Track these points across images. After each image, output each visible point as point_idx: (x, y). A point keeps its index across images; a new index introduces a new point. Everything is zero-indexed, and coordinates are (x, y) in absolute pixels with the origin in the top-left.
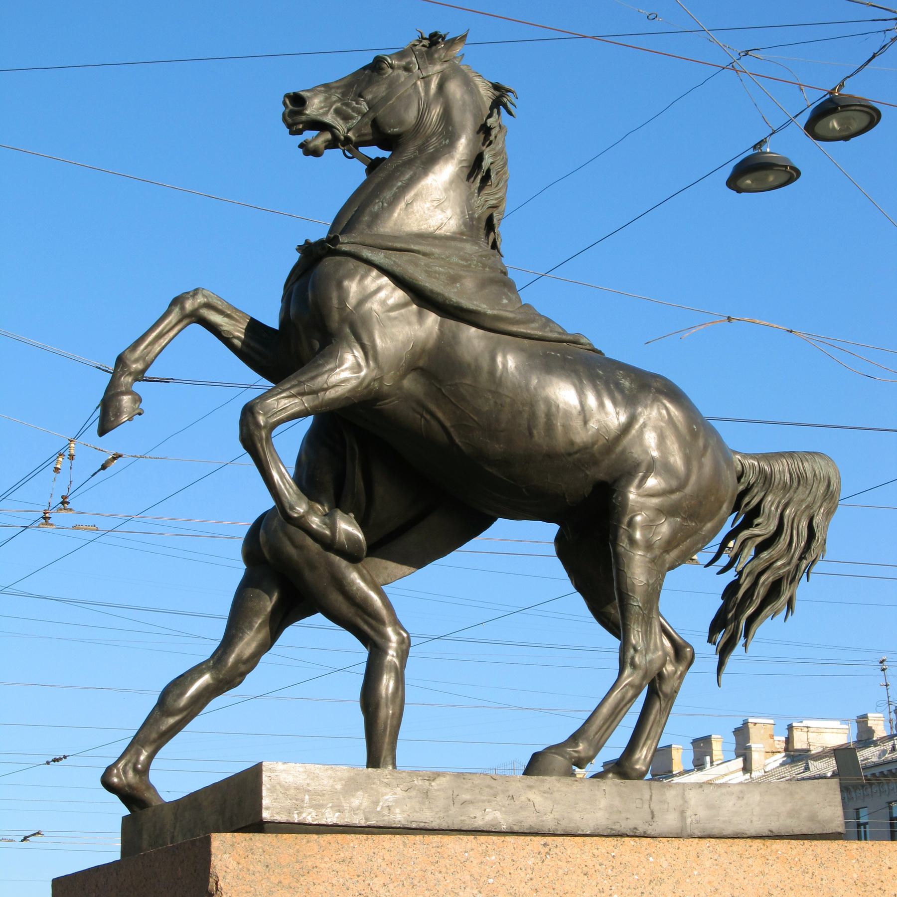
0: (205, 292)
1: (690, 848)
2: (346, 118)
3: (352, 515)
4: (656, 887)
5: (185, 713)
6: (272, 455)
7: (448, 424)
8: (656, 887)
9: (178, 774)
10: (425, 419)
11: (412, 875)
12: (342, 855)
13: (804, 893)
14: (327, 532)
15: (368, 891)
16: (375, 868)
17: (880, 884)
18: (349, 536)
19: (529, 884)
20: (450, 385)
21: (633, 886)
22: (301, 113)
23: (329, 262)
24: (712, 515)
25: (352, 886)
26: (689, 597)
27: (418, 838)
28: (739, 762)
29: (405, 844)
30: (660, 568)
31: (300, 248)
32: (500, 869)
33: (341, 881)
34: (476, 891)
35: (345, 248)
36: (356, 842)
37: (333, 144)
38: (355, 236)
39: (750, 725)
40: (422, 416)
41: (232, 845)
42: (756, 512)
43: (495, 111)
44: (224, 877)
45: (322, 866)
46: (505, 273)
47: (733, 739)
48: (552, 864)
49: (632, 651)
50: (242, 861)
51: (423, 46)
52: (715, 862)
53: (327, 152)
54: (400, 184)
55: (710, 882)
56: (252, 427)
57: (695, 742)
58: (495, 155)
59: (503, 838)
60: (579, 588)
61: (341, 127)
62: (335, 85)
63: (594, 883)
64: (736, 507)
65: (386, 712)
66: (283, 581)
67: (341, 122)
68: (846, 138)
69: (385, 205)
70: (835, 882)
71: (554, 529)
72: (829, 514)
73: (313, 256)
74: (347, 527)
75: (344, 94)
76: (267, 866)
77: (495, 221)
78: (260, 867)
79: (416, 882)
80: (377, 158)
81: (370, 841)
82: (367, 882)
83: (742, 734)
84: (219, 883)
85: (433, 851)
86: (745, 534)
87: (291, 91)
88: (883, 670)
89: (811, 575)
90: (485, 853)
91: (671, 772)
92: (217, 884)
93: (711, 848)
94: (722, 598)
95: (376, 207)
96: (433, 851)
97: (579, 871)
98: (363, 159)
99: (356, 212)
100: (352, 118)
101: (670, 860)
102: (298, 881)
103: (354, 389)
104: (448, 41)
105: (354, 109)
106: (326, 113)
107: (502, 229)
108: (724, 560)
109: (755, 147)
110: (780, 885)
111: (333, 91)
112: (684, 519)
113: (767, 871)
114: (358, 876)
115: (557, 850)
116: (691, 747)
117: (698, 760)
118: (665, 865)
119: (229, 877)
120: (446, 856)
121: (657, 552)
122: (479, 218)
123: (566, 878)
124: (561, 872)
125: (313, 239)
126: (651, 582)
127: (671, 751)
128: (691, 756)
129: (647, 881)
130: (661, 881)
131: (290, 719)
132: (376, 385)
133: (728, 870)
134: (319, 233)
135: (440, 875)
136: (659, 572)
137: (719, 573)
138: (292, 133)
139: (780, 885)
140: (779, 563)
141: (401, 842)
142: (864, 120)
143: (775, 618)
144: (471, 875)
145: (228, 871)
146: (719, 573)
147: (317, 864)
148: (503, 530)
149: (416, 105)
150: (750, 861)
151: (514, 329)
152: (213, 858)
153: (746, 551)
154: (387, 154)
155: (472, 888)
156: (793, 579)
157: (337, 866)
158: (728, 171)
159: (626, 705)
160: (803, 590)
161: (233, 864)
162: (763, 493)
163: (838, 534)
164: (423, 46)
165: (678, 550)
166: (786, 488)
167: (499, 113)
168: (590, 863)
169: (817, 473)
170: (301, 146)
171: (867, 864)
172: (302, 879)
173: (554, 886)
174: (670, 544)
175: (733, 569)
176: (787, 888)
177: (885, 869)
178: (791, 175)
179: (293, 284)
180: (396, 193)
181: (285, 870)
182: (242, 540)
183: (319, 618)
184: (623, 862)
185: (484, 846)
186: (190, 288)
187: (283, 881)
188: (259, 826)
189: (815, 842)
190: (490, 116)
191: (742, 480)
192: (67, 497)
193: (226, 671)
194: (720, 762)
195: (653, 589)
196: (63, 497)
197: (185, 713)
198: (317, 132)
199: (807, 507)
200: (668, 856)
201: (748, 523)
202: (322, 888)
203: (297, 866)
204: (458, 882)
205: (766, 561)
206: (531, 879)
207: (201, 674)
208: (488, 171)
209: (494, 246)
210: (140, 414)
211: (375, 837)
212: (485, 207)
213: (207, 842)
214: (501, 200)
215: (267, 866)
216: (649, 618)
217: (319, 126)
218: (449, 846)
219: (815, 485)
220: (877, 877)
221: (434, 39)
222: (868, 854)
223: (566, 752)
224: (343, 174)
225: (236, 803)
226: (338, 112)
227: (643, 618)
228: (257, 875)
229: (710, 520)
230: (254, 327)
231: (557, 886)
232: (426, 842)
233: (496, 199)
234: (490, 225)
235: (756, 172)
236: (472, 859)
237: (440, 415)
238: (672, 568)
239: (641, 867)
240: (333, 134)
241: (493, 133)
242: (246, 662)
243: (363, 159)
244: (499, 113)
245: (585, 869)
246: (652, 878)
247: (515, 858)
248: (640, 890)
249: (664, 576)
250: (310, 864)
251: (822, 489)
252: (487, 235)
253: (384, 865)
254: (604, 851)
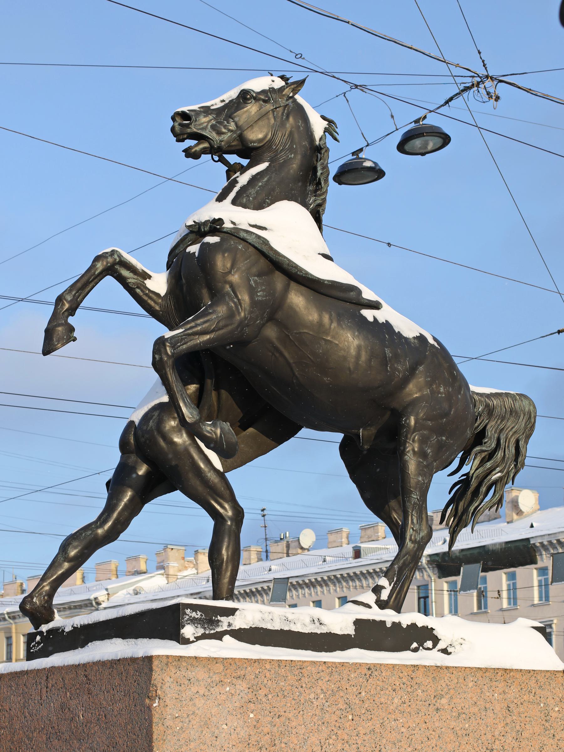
1: (460, 674)
7: (291, 361)
10: (275, 356)
12: (239, 673)
16: (260, 683)
19: (358, 696)
20: (296, 333)
40: (273, 354)
41: (167, 664)
48: (373, 683)
54: (260, 184)
66: (148, 467)
68: (423, 154)
70: (548, 700)
76: (189, 680)
79: (286, 694)
88: (264, 516)
93: (473, 674)
101: (447, 682)
104: (293, 83)
109: (353, 154)
113: (507, 691)
114: (249, 688)
115: (376, 673)
118: (444, 685)
120: (306, 675)
123: (382, 693)
124: (379, 688)
129: (433, 696)
130: (442, 696)
133: (483, 690)
135: (301, 689)
137: (449, 476)
138: (178, 141)
142: (439, 141)
146: (449, 476)
147: (222, 679)
172: (212, 690)
176: (519, 703)
183: (177, 496)
184: (418, 682)
185: (330, 669)
187: (200, 691)
198: (196, 142)
200: (446, 678)
203: (209, 680)
205: (488, 469)
214: (324, 200)
217: (200, 137)
228: (183, 686)
231: (376, 698)
236: (322, 678)
237: (286, 354)
239: (429, 686)
240: (210, 144)
245: (394, 687)
246: (435, 694)
248: (428, 702)
254: (406, 674)
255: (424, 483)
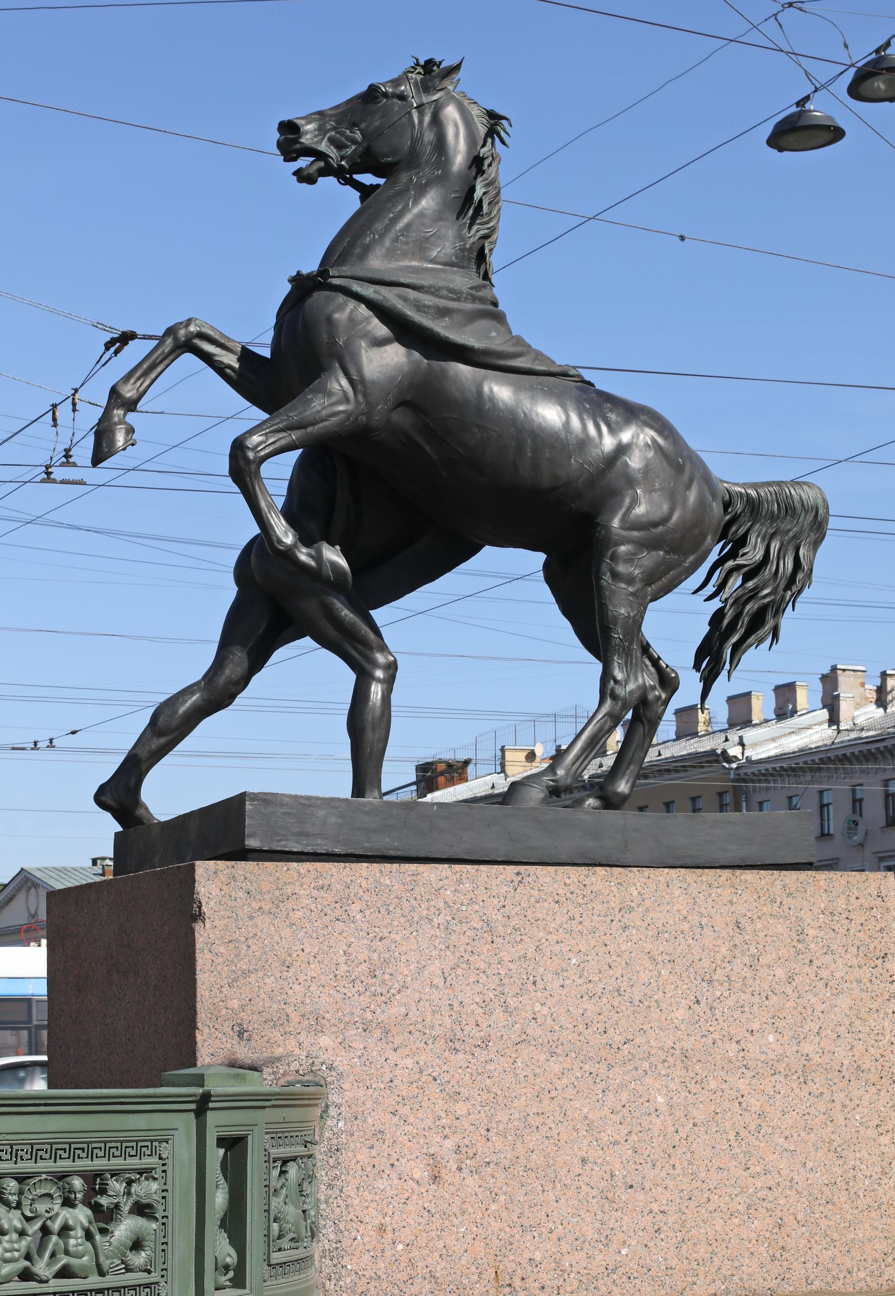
0: (198, 322)
2: (339, 146)
3: (338, 547)
4: (626, 915)
5: (176, 733)
6: (261, 490)
8: (626, 915)
9: (169, 793)
11: (388, 902)
12: (321, 882)
13: (771, 922)
14: (313, 563)
15: (345, 917)
16: (352, 895)
17: (847, 914)
18: (334, 566)
21: (602, 913)
22: (296, 141)
23: (319, 297)
24: (694, 548)
25: (329, 912)
26: (676, 623)
27: (395, 866)
28: (824, 714)
29: (381, 872)
30: (641, 604)
31: (291, 281)
32: (473, 896)
33: (320, 907)
34: (449, 918)
35: (336, 281)
36: (334, 870)
37: (327, 171)
38: (346, 270)
39: (839, 672)
41: (215, 873)
42: (742, 542)
43: (489, 140)
44: (207, 903)
45: (302, 892)
46: (495, 304)
47: (819, 686)
49: (612, 682)
50: (225, 888)
51: (419, 73)
52: (684, 892)
53: (320, 179)
54: (391, 215)
55: (679, 911)
56: (241, 462)
57: (778, 689)
58: (487, 185)
59: (476, 867)
60: (566, 613)
61: (332, 152)
62: (330, 112)
63: (565, 911)
64: (723, 535)
65: (370, 736)
66: (270, 609)
67: (335, 151)
69: (377, 236)
70: (803, 912)
71: (540, 558)
72: (816, 544)
73: (303, 287)
74: (333, 555)
75: (338, 123)
76: (249, 893)
77: (487, 251)
78: (241, 894)
79: (391, 908)
80: (371, 185)
81: (348, 869)
82: (344, 908)
83: (830, 680)
84: (203, 908)
85: (409, 879)
86: (730, 564)
87: (286, 118)
89: (796, 604)
90: (460, 882)
91: (751, 721)
92: (200, 910)
93: (681, 878)
94: (709, 625)
95: (368, 239)
96: (409, 879)
97: (551, 899)
98: (358, 186)
99: (346, 245)
100: (346, 147)
102: (278, 907)
103: (341, 424)
105: (347, 138)
106: (320, 142)
107: (495, 260)
108: (710, 589)
109: (798, 104)
110: (749, 915)
111: (327, 119)
112: (667, 552)
113: (735, 900)
114: (336, 902)
116: (773, 694)
117: (780, 709)
119: (212, 903)
121: (638, 586)
122: (471, 249)
123: (538, 905)
124: (533, 900)
125: (305, 271)
126: (632, 614)
127: (751, 699)
128: (773, 705)
129: (618, 909)
130: (631, 909)
131: (285, 732)
132: (364, 418)
134: (310, 265)
136: (640, 605)
137: (705, 600)
139: (748, 914)
140: (766, 592)
141: (377, 870)
143: (759, 647)
144: (445, 902)
145: (211, 897)
146: (705, 600)
148: (491, 558)
149: (410, 134)
150: (719, 890)
151: (502, 362)
152: (196, 885)
153: (731, 581)
154: (381, 181)
155: (446, 915)
156: (779, 611)
157: (315, 893)
158: (768, 129)
159: (604, 735)
160: (788, 621)
161: (215, 891)
162: (750, 523)
163: (827, 560)
164: (419, 73)
165: (661, 582)
166: (773, 518)
167: (493, 143)
168: (561, 892)
169: (805, 503)
170: (295, 174)
171: (834, 894)
172: (282, 905)
173: (526, 913)
174: (650, 578)
175: (718, 598)
176: (755, 917)
177: (852, 899)
178: (835, 134)
179: (284, 315)
180: (387, 225)
181: (265, 896)
182: (238, 553)
186: (183, 319)
188: (243, 854)
189: (785, 873)
190: (484, 146)
191: (730, 510)
192: (70, 450)
193: (217, 692)
194: (804, 711)
195: (634, 621)
196: (65, 450)
197: (176, 733)
199: (794, 537)
201: (733, 554)
202: (300, 914)
203: (277, 893)
204: (432, 909)
206: (504, 907)
207: (193, 693)
208: (481, 201)
209: (486, 277)
210: (133, 445)
211: (353, 865)
212: (477, 237)
213: (192, 869)
214: (493, 230)
215: (249, 893)
216: (629, 649)
218: (425, 875)
219: (803, 515)
220: (844, 906)
221: (429, 65)
222: (836, 884)
223: (543, 781)
224: (338, 202)
225: (223, 830)
226: (332, 141)
227: (624, 649)
228: (239, 900)
229: (693, 554)
230: (247, 355)
231: (529, 913)
232: (402, 870)
233: (488, 229)
234: (481, 257)
235: (797, 132)
238: (654, 599)
241: (487, 163)
242: (236, 683)
243: (358, 186)
244: (493, 143)
245: (557, 898)
246: (622, 906)
247: (488, 886)
248: (610, 918)
249: (645, 608)
250: (289, 891)
251: (810, 518)
252: (479, 267)
253: (361, 891)
255: (629, 617)
